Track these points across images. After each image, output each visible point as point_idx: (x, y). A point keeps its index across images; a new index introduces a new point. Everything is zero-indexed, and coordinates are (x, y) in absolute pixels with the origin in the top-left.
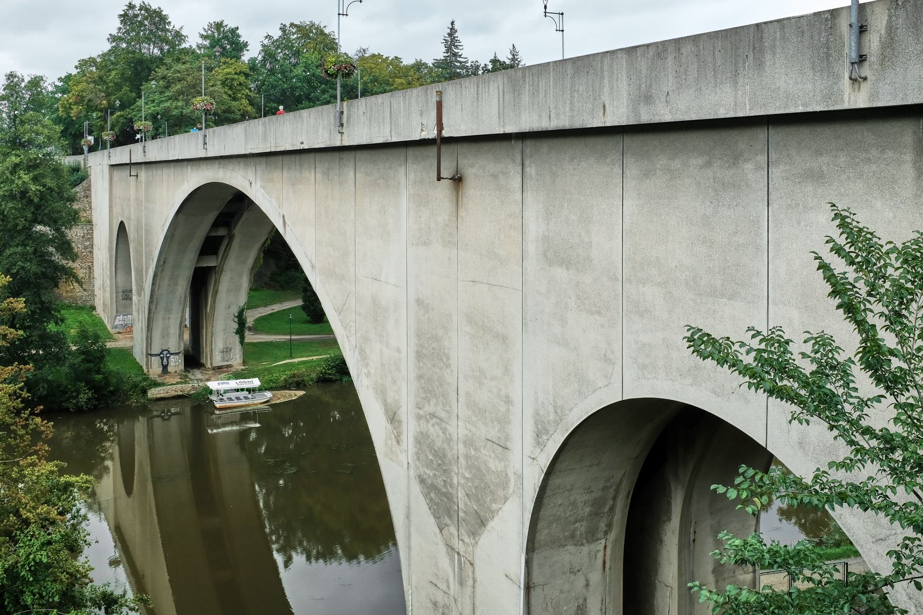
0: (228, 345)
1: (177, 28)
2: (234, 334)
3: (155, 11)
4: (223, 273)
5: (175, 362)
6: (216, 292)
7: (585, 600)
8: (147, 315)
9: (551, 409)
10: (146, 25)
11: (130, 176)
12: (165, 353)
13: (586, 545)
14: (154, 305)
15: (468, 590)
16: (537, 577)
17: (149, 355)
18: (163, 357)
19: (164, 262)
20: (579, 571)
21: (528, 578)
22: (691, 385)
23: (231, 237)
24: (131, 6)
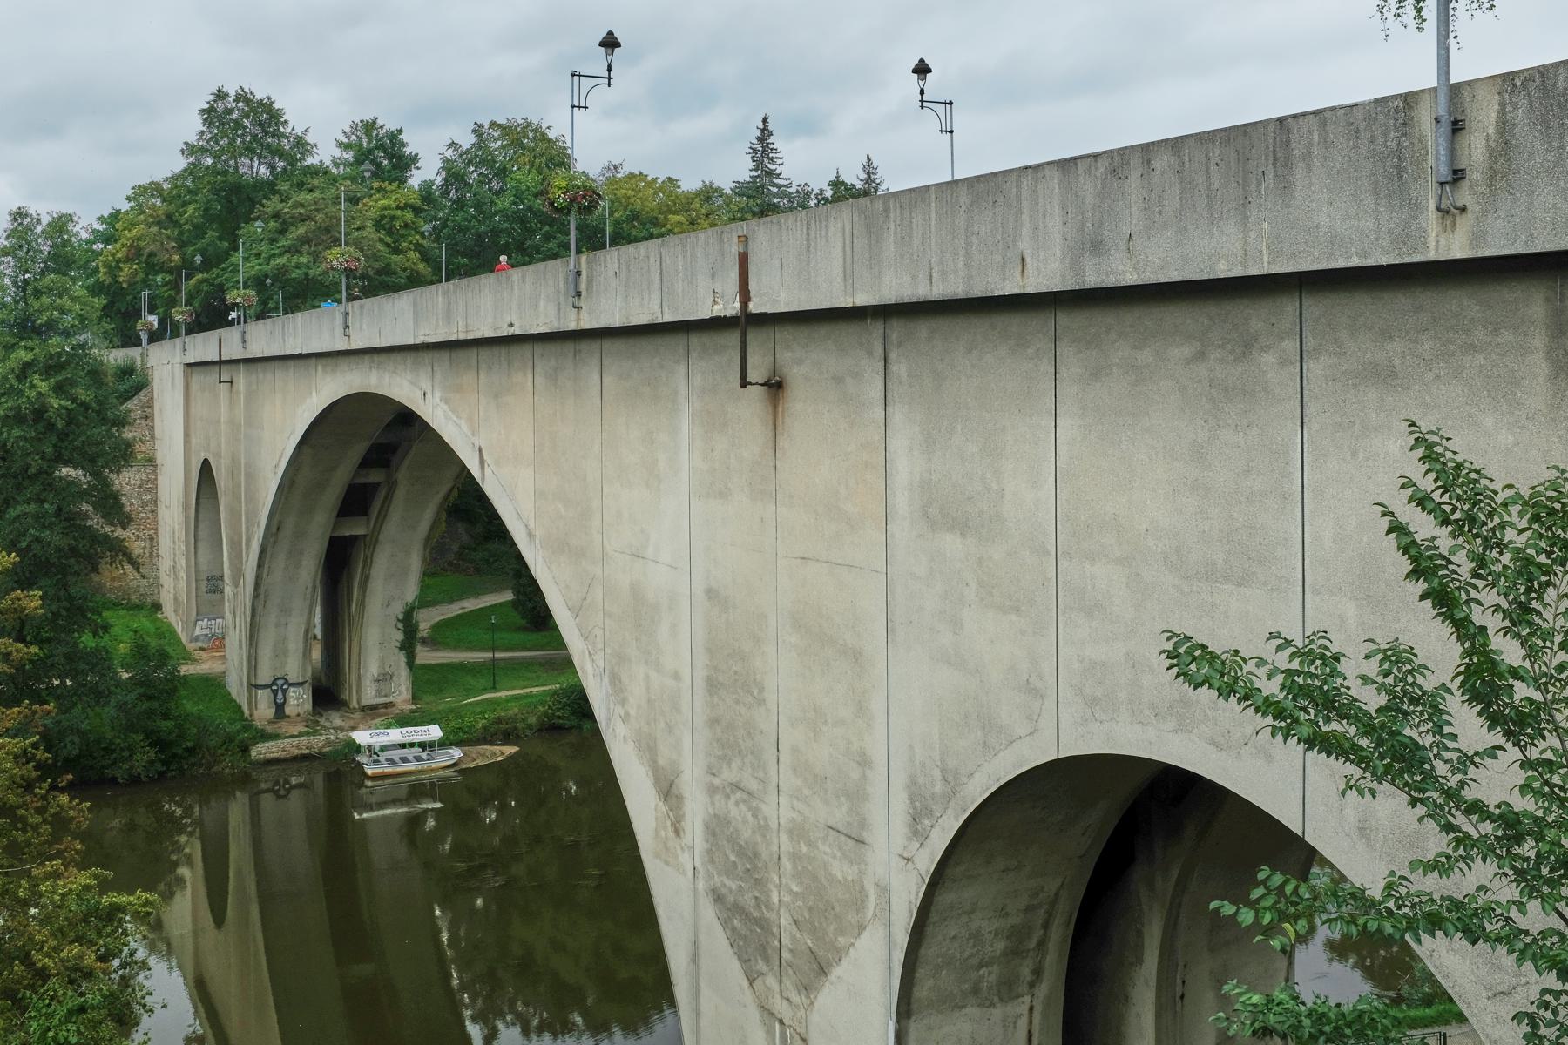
1: (299, 131)
2: (397, 650)
5: (298, 699)
6: (366, 579)
8: (248, 620)
9: (937, 773)
12: (280, 682)
17: (253, 686)
18: (277, 690)
22: (1175, 731)
23: (392, 486)
24: (221, 95)
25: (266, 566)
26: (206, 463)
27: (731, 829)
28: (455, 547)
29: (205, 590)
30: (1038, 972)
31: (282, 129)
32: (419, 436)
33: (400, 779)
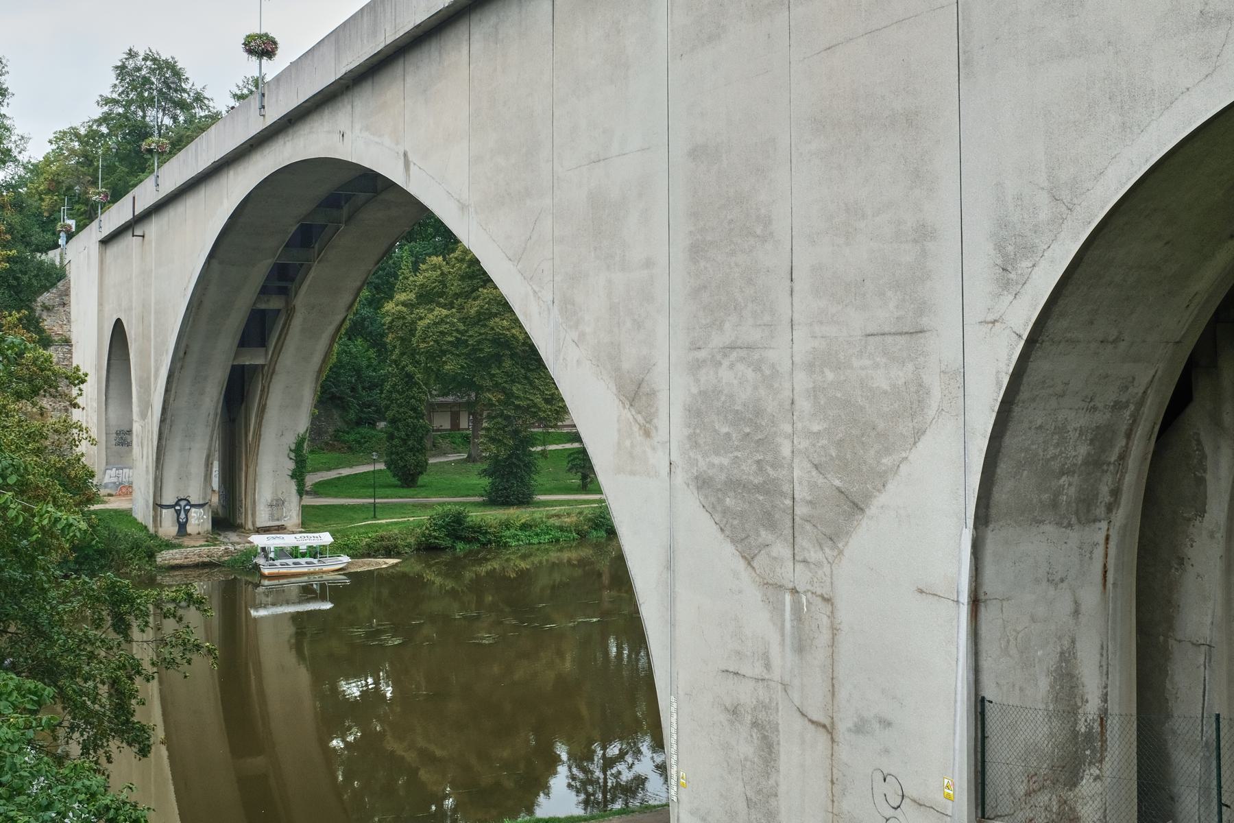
0: (280, 496)
1: (198, 87)
2: (289, 478)
3: (166, 62)
4: (274, 377)
5: (199, 519)
6: (262, 409)
7: (1073, 642)
8: (155, 443)
9: (1043, 198)
10: (153, 83)
11: (133, 236)
12: (183, 503)
13: (1076, 527)
14: (167, 426)
15: (819, 656)
16: (991, 584)
17: (158, 506)
18: (180, 510)
19: (185, 353)
20: (1062, 580)
21: (976, 581)
23: (290, 312)
24: (131, 54)
25: (173, 391)
26: (118, 323)
27: (723, 398)
28: (331, 430)
29: (114, 442)
30: (1116, 493)
31: (183, 85)
32: (319, 255)
33: (293, 580)
